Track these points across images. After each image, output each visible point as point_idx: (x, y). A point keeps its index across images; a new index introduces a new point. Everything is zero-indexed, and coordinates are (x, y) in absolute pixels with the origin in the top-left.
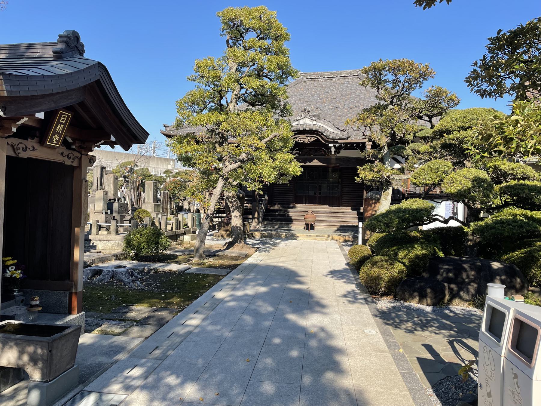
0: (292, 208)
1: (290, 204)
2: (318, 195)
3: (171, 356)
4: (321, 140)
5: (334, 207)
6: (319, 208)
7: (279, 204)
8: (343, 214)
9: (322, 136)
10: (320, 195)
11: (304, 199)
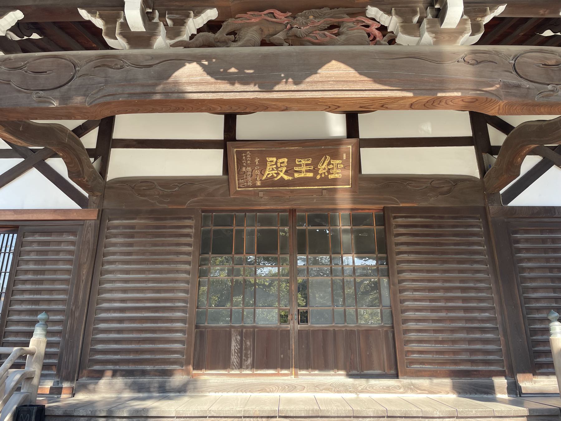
0: (182, 390)
1: (168, 373)
2: (294, 326)
5: (373, 382)
7: (115, 374)
10: (303, 326)
11: (234, 346)
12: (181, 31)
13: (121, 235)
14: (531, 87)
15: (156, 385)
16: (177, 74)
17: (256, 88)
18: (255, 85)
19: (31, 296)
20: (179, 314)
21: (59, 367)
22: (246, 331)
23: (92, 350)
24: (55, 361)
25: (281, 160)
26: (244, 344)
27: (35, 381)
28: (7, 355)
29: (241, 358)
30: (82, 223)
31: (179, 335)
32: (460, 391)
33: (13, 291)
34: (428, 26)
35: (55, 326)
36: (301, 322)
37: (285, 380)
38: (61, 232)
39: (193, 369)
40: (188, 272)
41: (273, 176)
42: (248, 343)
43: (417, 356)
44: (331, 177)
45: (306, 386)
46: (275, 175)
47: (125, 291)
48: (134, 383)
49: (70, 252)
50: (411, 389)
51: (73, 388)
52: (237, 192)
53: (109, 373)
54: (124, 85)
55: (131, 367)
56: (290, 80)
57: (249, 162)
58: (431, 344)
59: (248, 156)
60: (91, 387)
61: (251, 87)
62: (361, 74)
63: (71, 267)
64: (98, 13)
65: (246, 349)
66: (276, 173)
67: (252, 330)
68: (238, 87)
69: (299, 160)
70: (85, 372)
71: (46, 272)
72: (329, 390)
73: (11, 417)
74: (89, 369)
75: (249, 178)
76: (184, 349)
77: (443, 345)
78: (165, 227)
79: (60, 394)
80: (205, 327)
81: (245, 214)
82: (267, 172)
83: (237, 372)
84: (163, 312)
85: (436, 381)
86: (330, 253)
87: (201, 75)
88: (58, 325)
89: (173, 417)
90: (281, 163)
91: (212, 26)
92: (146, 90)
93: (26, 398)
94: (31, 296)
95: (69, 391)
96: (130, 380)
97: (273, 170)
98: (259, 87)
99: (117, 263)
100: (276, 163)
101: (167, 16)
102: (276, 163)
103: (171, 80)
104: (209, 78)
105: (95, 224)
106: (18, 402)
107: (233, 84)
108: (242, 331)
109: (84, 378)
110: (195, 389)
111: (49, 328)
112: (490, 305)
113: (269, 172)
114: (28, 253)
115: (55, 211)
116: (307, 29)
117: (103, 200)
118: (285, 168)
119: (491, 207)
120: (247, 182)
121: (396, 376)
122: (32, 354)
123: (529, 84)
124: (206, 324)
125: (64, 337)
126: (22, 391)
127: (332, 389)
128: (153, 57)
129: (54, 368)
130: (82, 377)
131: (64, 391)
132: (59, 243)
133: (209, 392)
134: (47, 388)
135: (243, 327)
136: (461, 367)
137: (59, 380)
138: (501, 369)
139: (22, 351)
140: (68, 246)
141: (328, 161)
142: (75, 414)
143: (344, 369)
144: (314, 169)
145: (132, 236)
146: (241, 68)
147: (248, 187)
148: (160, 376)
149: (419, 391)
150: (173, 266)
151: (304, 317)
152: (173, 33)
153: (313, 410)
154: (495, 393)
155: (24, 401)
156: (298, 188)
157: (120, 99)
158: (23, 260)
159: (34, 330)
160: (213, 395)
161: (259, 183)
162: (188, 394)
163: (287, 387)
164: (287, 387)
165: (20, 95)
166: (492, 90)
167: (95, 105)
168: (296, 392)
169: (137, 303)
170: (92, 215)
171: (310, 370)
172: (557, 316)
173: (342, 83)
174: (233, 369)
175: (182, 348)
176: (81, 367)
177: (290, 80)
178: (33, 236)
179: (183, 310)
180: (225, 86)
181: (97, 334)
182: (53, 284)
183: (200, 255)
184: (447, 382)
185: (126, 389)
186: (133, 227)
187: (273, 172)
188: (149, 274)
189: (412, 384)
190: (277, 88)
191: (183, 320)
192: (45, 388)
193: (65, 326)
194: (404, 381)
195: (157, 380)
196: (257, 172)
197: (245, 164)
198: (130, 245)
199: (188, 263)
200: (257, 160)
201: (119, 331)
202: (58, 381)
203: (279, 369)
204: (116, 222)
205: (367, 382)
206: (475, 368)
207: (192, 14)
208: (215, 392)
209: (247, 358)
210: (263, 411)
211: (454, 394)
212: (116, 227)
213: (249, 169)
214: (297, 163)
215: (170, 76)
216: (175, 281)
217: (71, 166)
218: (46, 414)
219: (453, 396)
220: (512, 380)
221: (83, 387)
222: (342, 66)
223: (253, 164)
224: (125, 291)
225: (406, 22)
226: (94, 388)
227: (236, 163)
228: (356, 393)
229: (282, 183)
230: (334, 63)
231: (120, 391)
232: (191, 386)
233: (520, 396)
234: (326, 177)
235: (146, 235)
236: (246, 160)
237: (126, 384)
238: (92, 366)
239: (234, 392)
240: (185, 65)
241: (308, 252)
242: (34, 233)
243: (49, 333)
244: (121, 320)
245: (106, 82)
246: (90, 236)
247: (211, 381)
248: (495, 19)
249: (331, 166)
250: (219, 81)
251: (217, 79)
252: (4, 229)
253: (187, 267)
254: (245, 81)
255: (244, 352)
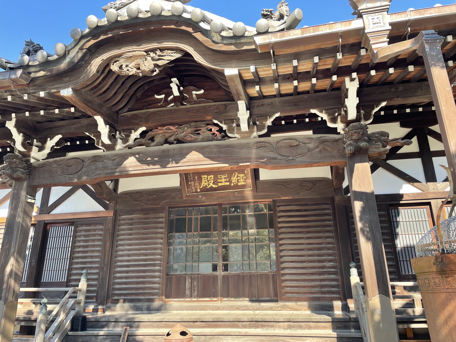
0: (158, 310)
1: (152, 300)
2: (220, 273)
3: (402, 55)
4: (198, 58)
5: (263, 304)
6: (224, 309)
7: (125, 301)
8: (290, 327)
9: (198, 36)
10: (226, 273)
11: (188, 285)
12: (129, 140)
13: (126, 224)
14: (282, 159)
15: (146, 307)
16: (125, 163)
17: (159, 167)
18: (159, 165)
19: (82, 260)
20: (157, 268)
21: (97, 297)
22: (194, 276)
23: (113, 288)
24: (95, 294)
25: (209, 177)
26: (193, 284)
27: (82, 304)
28: (66, 292)
29: (191, 291)
30: (106, 218)
31: (157, 279)
32: (313, 309)
33: (73, 257)
34: (236, 131)
35: (94, 276)
36: (224, 270)
37: (214, 304)
38: (96, 224)
39: (166, 298)
40: (161, 244)
41: (206, 185)
42: (195, 283)
43: (290, 289)
44: (239, 184)
45: (225, 307)
46: (208, 185)
47: (129, 255)
48: (134, 306)
49: (100, 235)
50: (284, 308)
51: (104, 309)
52: (187, 196)
53: (122, 301)
54: (104, 170)
55: (133, 297)
56: (174, 162)
57: (192, 179)
58: (298, 282)
59: (191, 175)
60: (112, 308)
61: (157, 166)
62: (205, 157)
63: (101, 243)
64: (93, 135)
65: (194, 286)
66: (208, 184)
67: (197, 276)
68: (151, 167)
69: (220, 176)
70: (110, 300)
71: (89, 247)
72: (238, 309)
73: (70, 322)
74: (112, 298)
75: (193, 188)
76: (160, 287)
77: (304, 282)
78: (149, 218)
79: (98, 312)
80: (173, 275)
81: (193, 208)
82: (203, 184)
83: (189, 299)
84: (149, 267)
85: (299, 303)
86: (241, 229)
87: (135, 162)
88: (96, 275)
89: (147, 322)
90: (210, 178)
91: (143, 134)
92: (113, 171)
93: (78, 313)
94: (82, 260)
95: (102, 310)
96: (132, 304)
97: (206, 182)
98: (160, 166)
99: (124, 240)
100: (207, 179)
101: (122, 133)
102: (207, 179)
103: (122, 166)
104: (139, 163)
105: (113, 219)
106: (74, 315)
107: (149, 166)
108: (192, 276)
109: (109, 304)
110: (166, 309)
111: (88, 277)
112: (334, 258)
113: (204, 183)
114: (80, 236)
115: (92, 212)
116: (184, 134)
117: (116, 205)
118: (213, 181)
119: (336, 197)
120: (192, 190)
121: (277, 301)
122: (80, 291)
123: (281, 157)
124: (172, 273)
125: (99, 282)
126: (76, 309)
127: (239, 308)
128: (116, 155)
129: (94, 298)
130: (108, 303)
131: (99, 310)
132: (95, 230)
133: (173, 310)
134: (91, 309)
135: (192, 274)
136: (315, 295)
137: (96, 304)
138: (339, 296)
139: (74, 289)
140: (99, 231)
141: (237, 175)
142: (100, 320)
143: (248, 297)
144: (229, 180)
145: (132, 224)
146: (152, 157)
147: (193, 192)
148: (148, 302)
149: (289, 309)
150: (153, 241)
151: (226, 268)
152: (125, 140)
153: (216, 318)
154: (334, 311)
155: (76, 315)
156: (221, 191)
157: (102, 176)
158: (77, 240)
159: (81, 278)
160: (175, 312)
161: (199, 190)
162: (162, 311)
163: (215, 308)
164: (215, 308)
165: (62, 177)
166: (263, 161)
167: (92, 179)
168: (220, 310)
169: (135, 262)
170: (110, 214)
171: (212, 298)
172: (354, 265)
173: (197, 162)
174: (187, 298)
175: (159, 287)
176: (108, 298)
177: (174, 162)
178: (82, 226)
179: (160, 265)
180: (146, 167)
181: (115, 280)
182: (93, 253)
183: (168, 233)
184: (306, 303)
185: (130, 309)
186: (132, 219)
187: (206, 183)
188: (141, 246)
189: (285, 305)
190: (168, 166)
191: (159, 271)
192: (90, 309)
193: (99, 276)
194: (280, 304)
195: (146, 304)
196: (197, 184)
197: (190, 180)
198: (131, 229)
199: (162, 238)
200: (196, 177)
201: (127, 278)
202: (96, 305)
203: (244, 298)
204: (124, 217)
205: (259, 304)
206: (323, 296)
207: (133, 131)
208: (177, 311)
209: (195, 291)
210: (191, 319)
211: (309, 311)
212: (124, 220)
213: (192, 182)
214: (219, 177)
215: (122, 164)
216: (155, 249)
217: (96, 190)
218: (87, 321)
219: (309, 312)
220: (344, 302)
221: (109, 308)
222: (197, 153)
223: (194, 180)
224: (129, 255)
225: (229, 127)
226: (114, 309)
227: (185, 180)
228: (253, 311)
229: (212, 189)
230: (193, 152)
231: (127, 310)
232: (163, 307)
233: (349, 313)
234: (237, 185)
235: (139, 223)
236: (190, 178)
237: (130, 307)
238: (113, 297)
239: (186, 310)
240: (128, 158)
241: (228, 229)
242: (82, 225)
243: (88, 280)
244: (127, 272)
245: (96, 169)
246: (110, 226)
247: (174, 305)
248: (276, 118)
249: (239, 178)
250: (143, 165)
251: (142, 164)
252: (67, 224)
253: (161, 241)
254: (154, 163)
255: (193, 288)
